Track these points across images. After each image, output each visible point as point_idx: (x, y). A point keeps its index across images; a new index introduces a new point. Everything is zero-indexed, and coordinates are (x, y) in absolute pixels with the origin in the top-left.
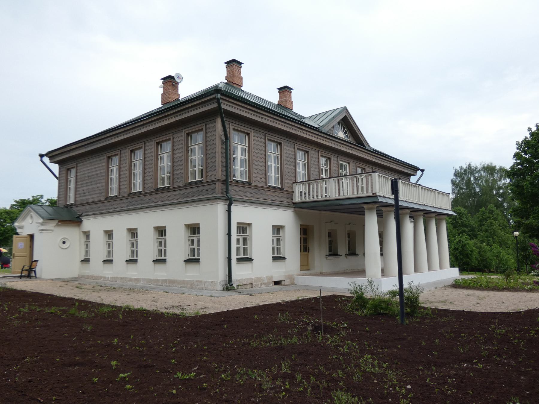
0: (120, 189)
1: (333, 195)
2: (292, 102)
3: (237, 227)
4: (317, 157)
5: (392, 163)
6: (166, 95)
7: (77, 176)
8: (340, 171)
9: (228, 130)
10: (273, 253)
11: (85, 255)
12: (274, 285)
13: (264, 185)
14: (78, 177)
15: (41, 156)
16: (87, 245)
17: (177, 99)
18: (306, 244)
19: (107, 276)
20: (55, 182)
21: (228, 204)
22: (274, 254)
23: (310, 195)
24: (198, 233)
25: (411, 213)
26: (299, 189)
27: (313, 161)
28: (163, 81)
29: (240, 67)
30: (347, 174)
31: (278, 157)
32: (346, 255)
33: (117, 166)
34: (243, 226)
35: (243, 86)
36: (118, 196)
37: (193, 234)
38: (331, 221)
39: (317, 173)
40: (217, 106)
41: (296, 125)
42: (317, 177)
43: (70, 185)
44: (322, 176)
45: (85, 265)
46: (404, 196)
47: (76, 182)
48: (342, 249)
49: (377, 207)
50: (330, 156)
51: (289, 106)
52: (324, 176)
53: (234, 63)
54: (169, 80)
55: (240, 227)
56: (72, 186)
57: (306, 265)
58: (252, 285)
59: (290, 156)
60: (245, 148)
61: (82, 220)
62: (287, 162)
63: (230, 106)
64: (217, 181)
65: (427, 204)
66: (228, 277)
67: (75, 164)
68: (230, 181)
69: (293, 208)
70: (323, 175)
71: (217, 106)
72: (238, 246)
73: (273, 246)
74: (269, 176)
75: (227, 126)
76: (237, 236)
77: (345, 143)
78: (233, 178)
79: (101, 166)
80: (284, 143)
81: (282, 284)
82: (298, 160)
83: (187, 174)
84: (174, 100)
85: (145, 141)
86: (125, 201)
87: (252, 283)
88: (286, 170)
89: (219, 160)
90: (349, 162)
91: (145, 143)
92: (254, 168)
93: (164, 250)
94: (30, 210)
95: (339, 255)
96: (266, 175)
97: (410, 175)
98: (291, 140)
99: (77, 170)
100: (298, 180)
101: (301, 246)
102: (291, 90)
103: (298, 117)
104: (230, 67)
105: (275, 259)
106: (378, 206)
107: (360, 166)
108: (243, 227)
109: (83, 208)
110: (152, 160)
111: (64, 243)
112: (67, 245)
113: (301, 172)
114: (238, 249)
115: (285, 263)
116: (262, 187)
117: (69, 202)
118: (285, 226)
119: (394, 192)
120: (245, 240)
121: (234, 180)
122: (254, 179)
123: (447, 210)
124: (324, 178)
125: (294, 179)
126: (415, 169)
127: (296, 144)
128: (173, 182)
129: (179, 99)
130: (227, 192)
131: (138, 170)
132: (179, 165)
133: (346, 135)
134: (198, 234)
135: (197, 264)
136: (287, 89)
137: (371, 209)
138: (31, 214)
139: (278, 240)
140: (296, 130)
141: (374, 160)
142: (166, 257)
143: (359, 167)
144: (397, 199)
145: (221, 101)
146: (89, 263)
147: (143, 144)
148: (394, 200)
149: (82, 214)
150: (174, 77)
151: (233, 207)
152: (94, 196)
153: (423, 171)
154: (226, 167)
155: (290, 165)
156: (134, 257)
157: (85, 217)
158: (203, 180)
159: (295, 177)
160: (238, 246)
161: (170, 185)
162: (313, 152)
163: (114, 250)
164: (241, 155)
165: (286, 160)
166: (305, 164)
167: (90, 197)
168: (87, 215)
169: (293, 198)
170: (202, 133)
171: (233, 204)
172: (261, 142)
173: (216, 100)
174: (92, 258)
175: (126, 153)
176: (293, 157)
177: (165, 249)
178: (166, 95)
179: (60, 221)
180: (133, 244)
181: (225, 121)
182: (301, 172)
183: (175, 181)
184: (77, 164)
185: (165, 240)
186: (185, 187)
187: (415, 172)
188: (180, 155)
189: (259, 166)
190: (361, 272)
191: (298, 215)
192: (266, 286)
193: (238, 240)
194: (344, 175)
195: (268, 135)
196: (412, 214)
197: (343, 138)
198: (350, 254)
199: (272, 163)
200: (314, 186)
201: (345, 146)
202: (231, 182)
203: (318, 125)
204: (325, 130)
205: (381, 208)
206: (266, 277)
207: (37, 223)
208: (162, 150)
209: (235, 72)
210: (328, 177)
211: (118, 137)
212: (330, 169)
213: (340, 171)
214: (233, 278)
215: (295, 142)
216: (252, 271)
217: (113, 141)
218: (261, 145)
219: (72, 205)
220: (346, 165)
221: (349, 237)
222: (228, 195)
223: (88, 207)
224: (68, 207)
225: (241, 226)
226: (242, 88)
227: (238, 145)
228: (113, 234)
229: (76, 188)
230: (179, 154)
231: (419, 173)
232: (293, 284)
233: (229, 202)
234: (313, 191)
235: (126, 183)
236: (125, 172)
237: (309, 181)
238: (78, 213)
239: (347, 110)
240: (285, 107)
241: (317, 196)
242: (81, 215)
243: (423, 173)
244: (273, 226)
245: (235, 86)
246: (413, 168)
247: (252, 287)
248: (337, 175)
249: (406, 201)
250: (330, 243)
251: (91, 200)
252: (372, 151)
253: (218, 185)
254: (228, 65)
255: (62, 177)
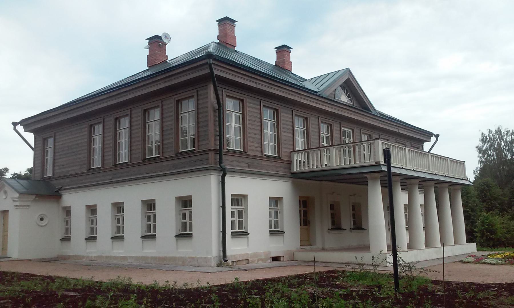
0: (103, 160)
1: (335, 164)
2: (291, 62)
3: (232, 199)
4: (317, 123)
5: (402, 129)
6: (153, 57)
7: (55, 146)
8: (343, 138)
9: (221, 97)
10: (271, 227)
11: (65, 232)
12: (272, 261)
13: (259, 154)
14: (57, 147)
15: (15, 124)
16: (67, 222)
17: (164, 61)
18: (307, 217)
19: (90, 255)
20: (31, 153)
21: (221, 174)
22: (272, 228)
23: (301, 164)
24: (190, 206)
25: (421, 183)
26: (297, 158)
27: (313, 129)
28: (149, 41)
29: (234, 25)
30: (351, 141)
31: (274, 124)
32: (350, 229)
33: (101, 135)
34: (237, 198)
35: (236, 26)
36: (102, 167)
37: (185, 208)
38: (333, 193)
39: (318, 141)
40: (210, 72)
41: (294, 90)
42: (318, 146)
43: (47, 157)
44: (322, 143)
45: (65, 243)
46: (402, 163)
47: (54, 153)
48: (347, 222)
49: (381, 177)
50: (332, 122)
51: (287, 67)
52: (325, 144)
53: (228, 22)
54: (155, 40)
55: (235, 199)
56: (50, 157)
57: (308, 240)
58: (248, 261)
59: (287, 123)
60: (240, 116)
61: (62, 194)
62: (285, 130)
63: (223, 72)
64: (211, 150)
65: (438, 173)
66: (222, 252)
67: (53, 133)
68: (224, 150)
69: (291, 179)
70: (324, 143)
71: (210, 72)
72: (233, 219)
73: (271, 219)
74: (265, 144)
75: (220, 93)
76: (232, 208)
77: (348, 108)
78: (227, 148)
79: (83, 136)
80: (281, 110)
81: (280, 260)
82: (296, 127)
83: (178, 144)
84: (161, 62)
85: (131, 108)
86: (110, 173)
87: (248, 259)
88: (283, 138)
89: (212, 129)
90: (352, 128)
91: (131, 110)
92: (250, 137)
93: (153, 225)
94: (4, 184)
95: (343, 229)
96: (262, 144)
97: (423, 142)
98: (288, 106)
99: (55, 140)
100: (297, 149)
101: (300, 219)
102: (290, 50)
103: (297, 80)
104: (223, 25)
105: (272, 233)
106: (381, 175)
107: (366, 133)
108: (238, 200)
109: (62, 181)
110: (140, 128)
111: (42, 219)
112: (43, 223)
113: (300, 138)
114: (233, 223)
115: (283, 238)
116: (258, 156)
117: (46, 175)
118: (283, 198)
119: (386, 161)
120: (240, 214)
121: (227, 149)
122: (249, 148)
123: (463, 179)
124: (325, 146)
125: (292, 147)
126: (428, 135)
127: (294, 111)
128: (163, 153)
129: (167, 61)
130: (220, 162)
131: (124, 139)
132: (169, 134)
133: (350, 99)
134: (190, 207)
135: (187, 239)
136: (286, 49)
137: (374, 179)
138: (5, 189)
139: (276, 213)
140: (294, 95)
141: (381, 126)
142: (155, 232)
143: (364, 133)
144: (389, 167)
145: (213, 66)
146: (69, 242)
147: (129, 112)
148: (386, 167)
149: (61, 188)
150: (161, 37)
151: (227, 178)
152: (75, 168)
153: (437, 136)
154: (220, 136)
155: (287, 133)
156: (120, 234)
157: (65, 191)
158: (194, 150)
159: (294, 145)
160: (233, 219)
161: (159, 155)
162: (313, 118)
163: (97, 226)
164: (235, 123)
165: (284, 128)
166: (304, 131)
167: (70, 169)
168: (69, 189)
169: (291, 168)
170: (193, 99)
171: (227, 175)
172: (256, 109)
173: (208, 66)
174: (73, 235)
175: (110, 121)
176: (291, 124)
177: (154, 224)
178: (153, 57)
179: (37, 195)
180: (119, 220)
181: (218, 88)
182: (300, 138)
183: (164, 151)
184: (55, 133)
185: (154, 214)
186: (176, 157)
187: (429, 138)
188: (170, 123)
189: (255, 134)
190: (366, 248)
191: (296, 187)
192: (263, 262)
193: (233, 213)
194: (347, 142)
195: (263, 101)
196: (406, 182)
197: (346, 102)
198: (354, 229)
199: (269, 132)
200: (314, 155)
201: (348, 111)
202: (226, 152)
203: (318, 89)
204: (326, 94)
205: (436, 185)
206: (263, 252)
207: (12, 198)
208: (150, 118)
209: (228, 31)
210: (329, 144)
211: (101, 103)
212: (332, 136)
213: (343, 138)
214: (228, 253)
215: (293, 108)
216: (248, 245)
217: (95, 108)
218: (256, 112)
219: (50, 178)
220: (350, 132)
221: (353, 209)
222: (222, 165)
223: (67, 180)
224: (45, 181)
225: (236, 198)
226: (236, 49)
227: (232, 112)
228: (96, 209)
229: (54, 159)
230: (170, 122)
231: (433, 139)
232: (293, 260)
233: (223, 172)
234: (313, 160)
235: (111, 153)
236: (110, 142)
237: (308, 149)
238: (57, 187)
239: (350, 72)
240: (283, 68)
241: (317, 166)
242: (60, 189)
243: (437, 140)
244: (270, 198)
245: (228, 46)
246: (427, 133)
247: (248, 263)
248: (339, 143)
249: (413, 170)
250: (333, 216)
251: (70, 173)
252: (379, 115)
253: (211, 155)
254: (220, 23)
255: (37, 147)
